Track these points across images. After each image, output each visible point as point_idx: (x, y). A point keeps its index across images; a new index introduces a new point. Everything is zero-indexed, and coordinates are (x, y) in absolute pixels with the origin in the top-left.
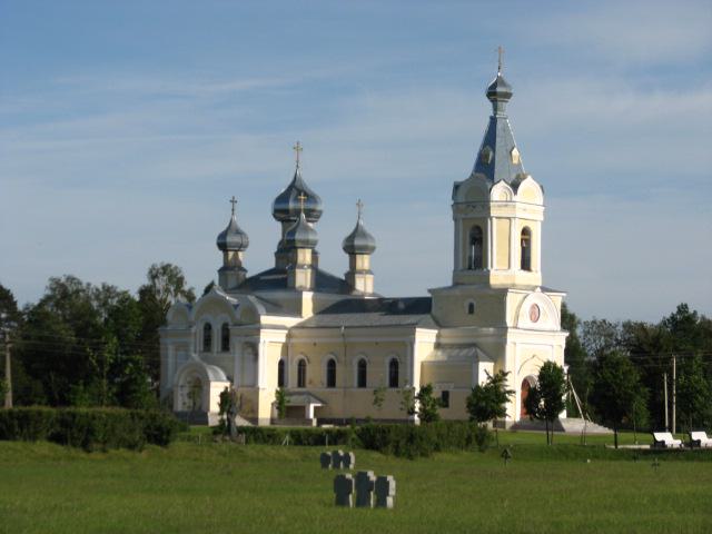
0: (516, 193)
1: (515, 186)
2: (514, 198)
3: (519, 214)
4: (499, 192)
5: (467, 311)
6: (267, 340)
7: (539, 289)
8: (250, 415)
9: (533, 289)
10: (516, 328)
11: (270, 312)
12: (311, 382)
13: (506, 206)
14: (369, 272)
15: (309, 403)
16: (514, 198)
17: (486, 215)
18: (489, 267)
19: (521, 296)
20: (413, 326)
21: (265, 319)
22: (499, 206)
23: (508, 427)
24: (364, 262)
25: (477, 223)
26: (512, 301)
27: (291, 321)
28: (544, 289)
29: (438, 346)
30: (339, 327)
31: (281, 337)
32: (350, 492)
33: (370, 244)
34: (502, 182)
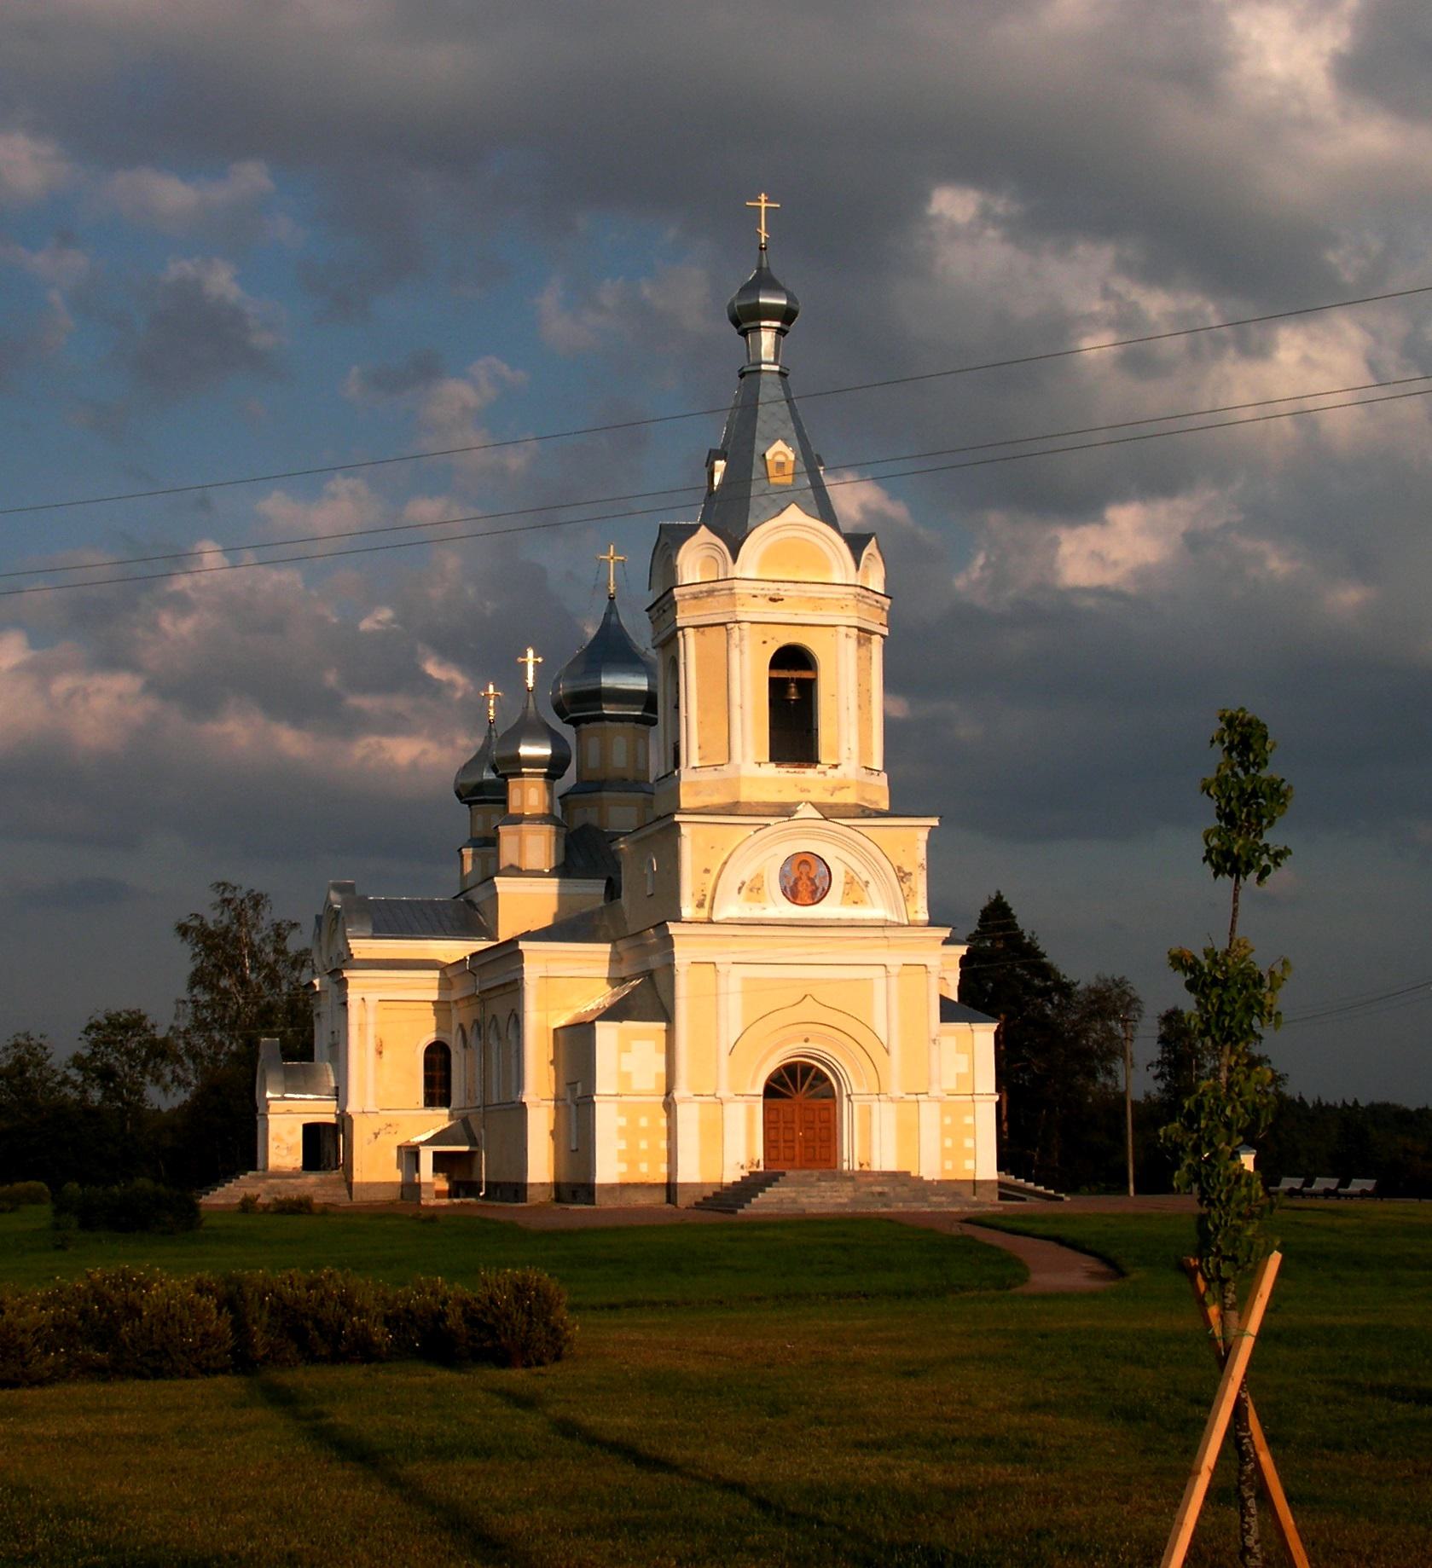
6: (372, 998)
7: (806, 811)
13: (710, 593)
21: (362, 947)
22: (695, 597)
31: (426, 986)
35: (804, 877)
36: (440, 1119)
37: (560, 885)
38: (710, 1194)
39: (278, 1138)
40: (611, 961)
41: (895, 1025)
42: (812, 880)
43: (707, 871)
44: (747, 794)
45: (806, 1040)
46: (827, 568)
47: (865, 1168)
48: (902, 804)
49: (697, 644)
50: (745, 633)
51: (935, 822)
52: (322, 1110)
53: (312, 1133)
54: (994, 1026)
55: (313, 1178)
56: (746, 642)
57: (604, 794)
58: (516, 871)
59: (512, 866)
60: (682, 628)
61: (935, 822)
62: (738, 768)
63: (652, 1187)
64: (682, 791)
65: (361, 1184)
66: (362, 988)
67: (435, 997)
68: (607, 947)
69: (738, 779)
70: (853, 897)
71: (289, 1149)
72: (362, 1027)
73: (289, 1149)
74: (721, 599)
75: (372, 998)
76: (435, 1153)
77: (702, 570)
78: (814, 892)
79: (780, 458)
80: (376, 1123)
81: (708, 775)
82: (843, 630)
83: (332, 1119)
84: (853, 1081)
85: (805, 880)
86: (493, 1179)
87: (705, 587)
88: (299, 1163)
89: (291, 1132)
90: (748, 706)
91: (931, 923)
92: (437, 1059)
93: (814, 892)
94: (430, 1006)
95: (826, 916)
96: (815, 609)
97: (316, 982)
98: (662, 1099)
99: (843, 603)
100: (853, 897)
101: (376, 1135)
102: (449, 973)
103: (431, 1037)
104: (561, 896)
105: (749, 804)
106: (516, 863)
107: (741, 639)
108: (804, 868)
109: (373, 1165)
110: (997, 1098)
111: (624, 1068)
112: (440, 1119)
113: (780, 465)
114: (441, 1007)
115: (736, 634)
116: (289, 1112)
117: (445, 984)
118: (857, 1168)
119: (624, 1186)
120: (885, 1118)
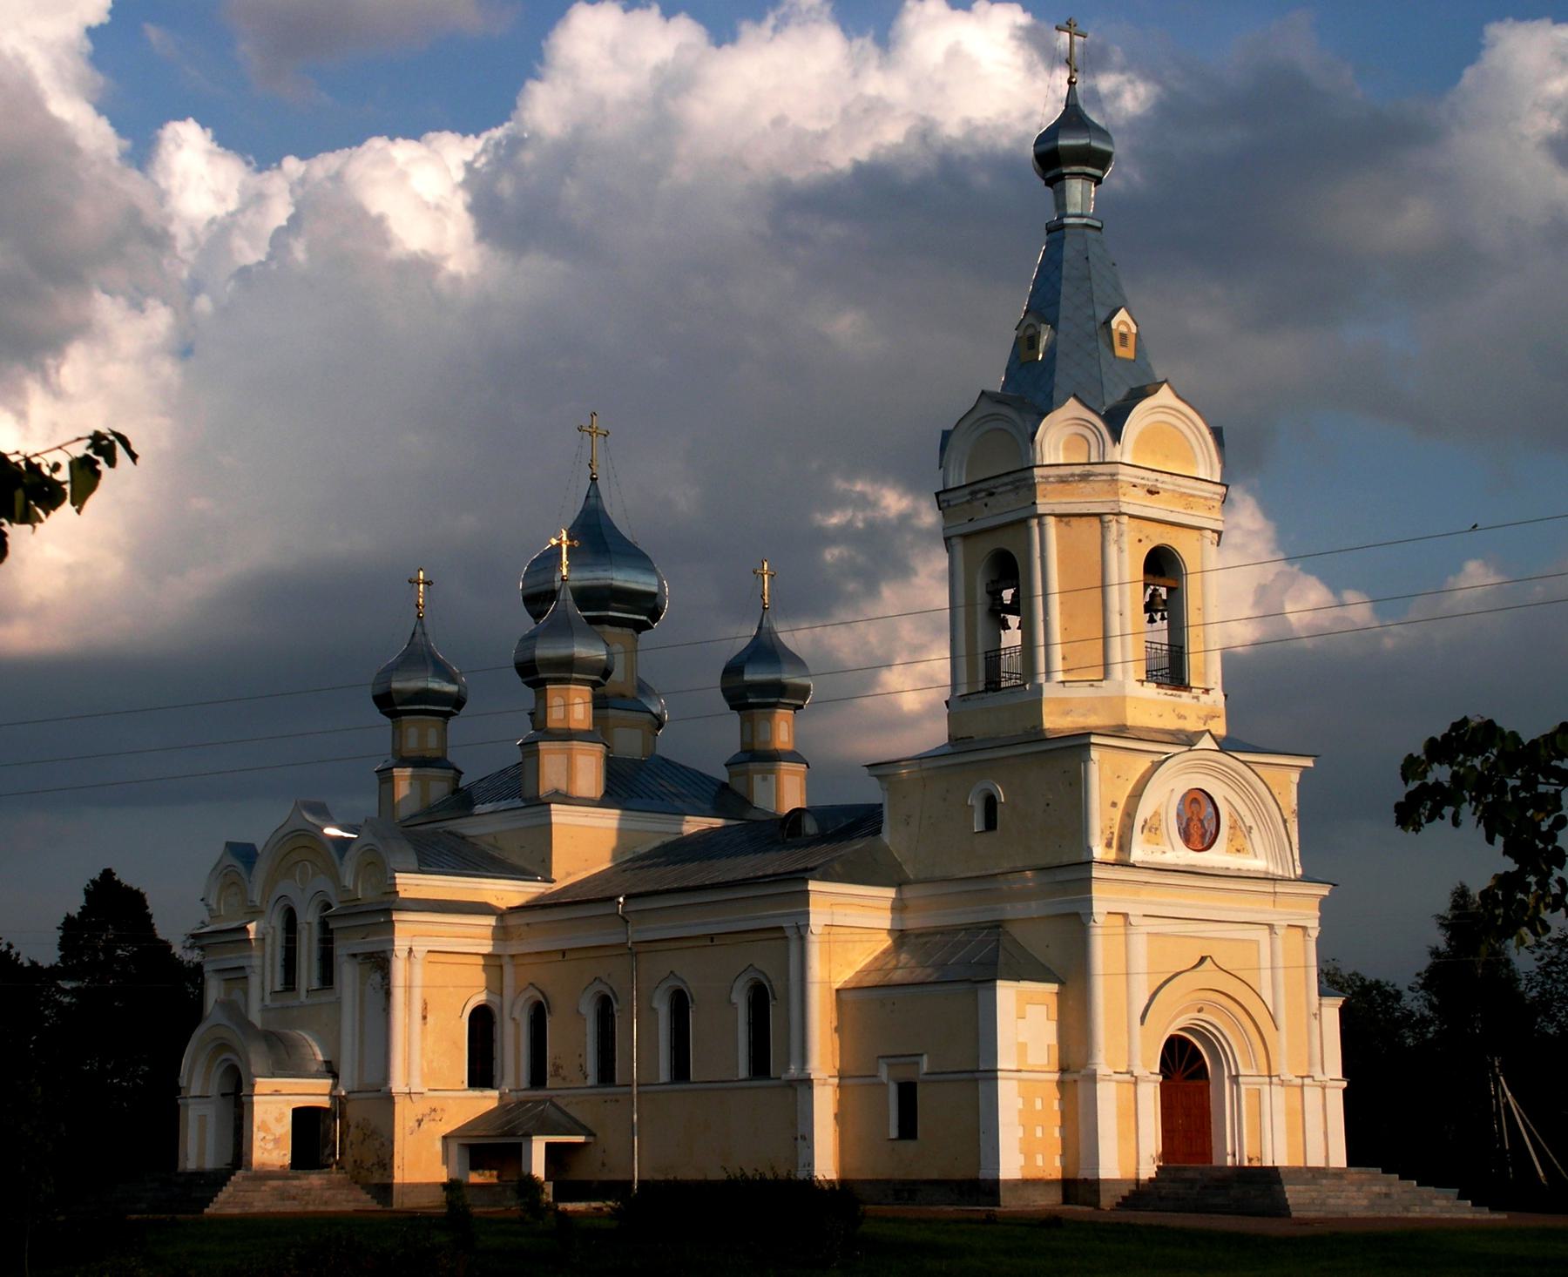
0: (1116, 436)
1: (1115, 420)
2: (1114, 453)
3: (1134, 502)
4: (1059, 438)
5: (978, 825)
6: (420, 948)
7: (1207, 742)
8: (376, 1178)
9: (1188, 740)
10: (1123, 863)
11: (427, 864)
12: (557, 1068)
13: (1084, 477)
14: (794, 757)
15: (528, 1136)
16: (1114, 453)
17: (1023, 522)
18: (1042, 679)
19: (1144, 763)
20: (801, 876)
21: (410, 884)
22: (1062, 480)
23: (1106, 1201)
24: (783, 730)
25: (1004, 541)
26: (1106, 778)
27: (507, 892)
28: (1225, 745)
29: (901, 937)
30: (612, 899)
31: (477, 935)
32: (1493, 1209)
33: (790, 677)
34: (1072, 402)
35: (1195, 821)
36: (487, 1101)
37: (621, 819)
38: (1126, 1193)
39: (265, 1127)
40: (893, 909)
41: (1281, 991)
42: (1201, 821)
43: (1114, 805)
44: (1135, 718)
45: (1200, 1010)
46: (1191, 460)
47: (1255, 1164)
48: (1077, 745)
49: (1060, 537)
50: (1125, 528)
51: (1309, 763)
52: (315, 1092)
53: (305, 1120)
54: (1339, 1001)
55: (315, 1179)
56: (1125, 539)
57: (611, 712)
58: (567, 799)
59: (557, 792)
60: (1041, 516)
61: (1309, 763)
62: (1122, 685)
63: (1049, 1183)
64: (1045, 709)
65: (403, 1185)
66: (412, 937)
67: (487, 948)
68: (890, 893)
69: (1124, 698)
70: (1237, 844)
71: (277, 1141)
72: (409, 988)
73: (277, 1141)
74: (1097, 486)
75: (420, 948)
76: (548, 1145)
77: (1067, 448)
78: (1203, 836)
79: (1123, 329)
80: (420, 1108)
81: (1081, 692)
82: (1208, 533)
83: (324, 1102)
84: (1242, 1057)
85: (1200, 822)
86: (646, 1177)
87: (1078, 470)
88: (287, 1160)
89: (279, 1120)
90: (1128, 613)
91: (1305, 878)
92: (482, 1023)
93: (1203, 836)
94: (481, 961)
95: (1216, 865)
96: (1188, 506)
97: (252, 927)
98: (1056, 1076)
99: (1211, 503)
100: (1237, 844)
101: (420, 1122)
102: (506, 918)
103: (480, 998)
104: (621, 832)
105: (1133, 728)
106: (563, 787)
107: (1120, 535)
108: (1195, 806)
109: (420, 1162)
110: (1345, 1084)
111: (1021, 1039)
112: (487, 1101)
113: (1123, 337)
114: (493, 963)
115: (1114, 527)
116: (277, 1093)
117: (502, 933)
118: (1246, 1163)
119: (1025, 1183)
120: (1276, 1101)
